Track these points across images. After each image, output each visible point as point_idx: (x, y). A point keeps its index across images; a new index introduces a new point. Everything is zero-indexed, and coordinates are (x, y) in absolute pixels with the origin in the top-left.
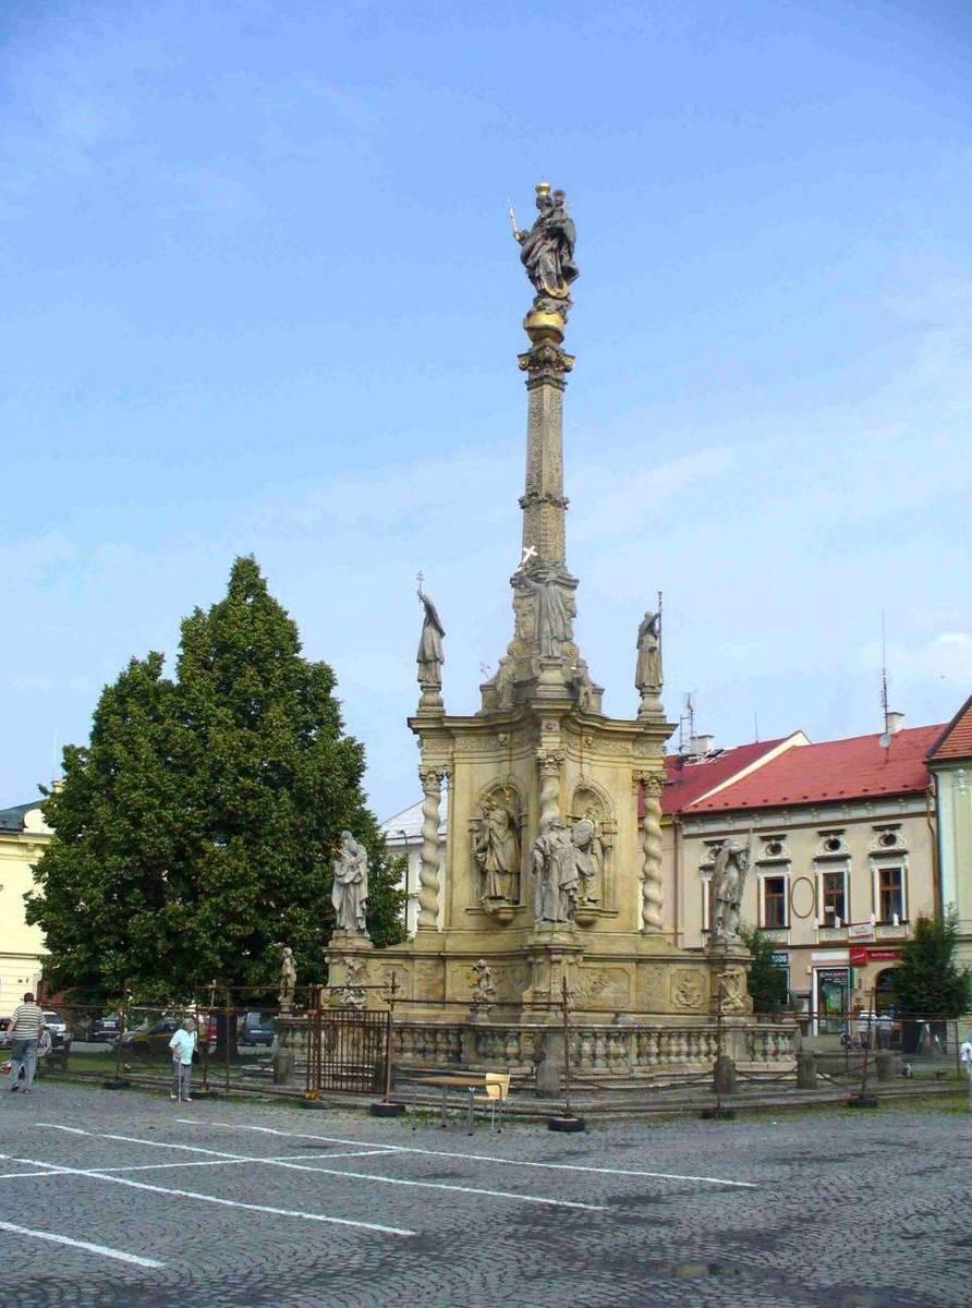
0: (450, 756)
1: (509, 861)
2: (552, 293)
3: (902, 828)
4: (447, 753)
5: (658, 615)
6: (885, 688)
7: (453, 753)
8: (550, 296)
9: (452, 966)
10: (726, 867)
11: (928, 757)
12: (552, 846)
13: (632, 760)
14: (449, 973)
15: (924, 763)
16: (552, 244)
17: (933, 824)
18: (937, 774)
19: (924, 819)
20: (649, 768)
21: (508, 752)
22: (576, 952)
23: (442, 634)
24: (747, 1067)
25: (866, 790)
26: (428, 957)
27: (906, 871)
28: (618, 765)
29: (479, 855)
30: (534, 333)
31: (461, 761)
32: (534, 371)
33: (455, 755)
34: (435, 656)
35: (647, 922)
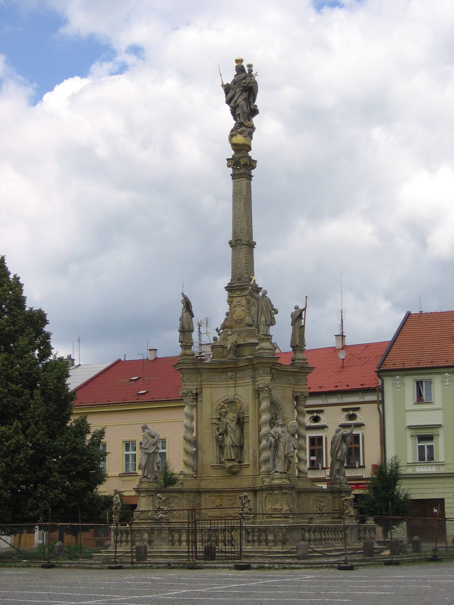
0: (199, 383)
1: (237, 441)
2: (246, 124)
3: (361, 410)
4: (198, 382)
5: (305, 309)
6: (342, 321)
7: (201, 382)
8: (245, 126)
9: (204, 497)
10: (341, 443)
11: (378, 368)
12: (279, 434)
13: (292, 386)
14: (203, 500)
15: (376, 371)
16: (245, 95)
17: (381, 407)
18: (383, 378)
19: (376, 405)
20: (300, 390)
21: (234, 382)
22: (293, 488)
23: (193, 316)
24: (358, 546)
25: (336, 386)
26: (192, 492)
27: (363, 436)
28: (285, 388)
29: (220, 437)
30: (234, 147)
31: (206, 386)
32: (236, 169)
33: (203, 383)
34: (190, 329)
35: (300, 471)
